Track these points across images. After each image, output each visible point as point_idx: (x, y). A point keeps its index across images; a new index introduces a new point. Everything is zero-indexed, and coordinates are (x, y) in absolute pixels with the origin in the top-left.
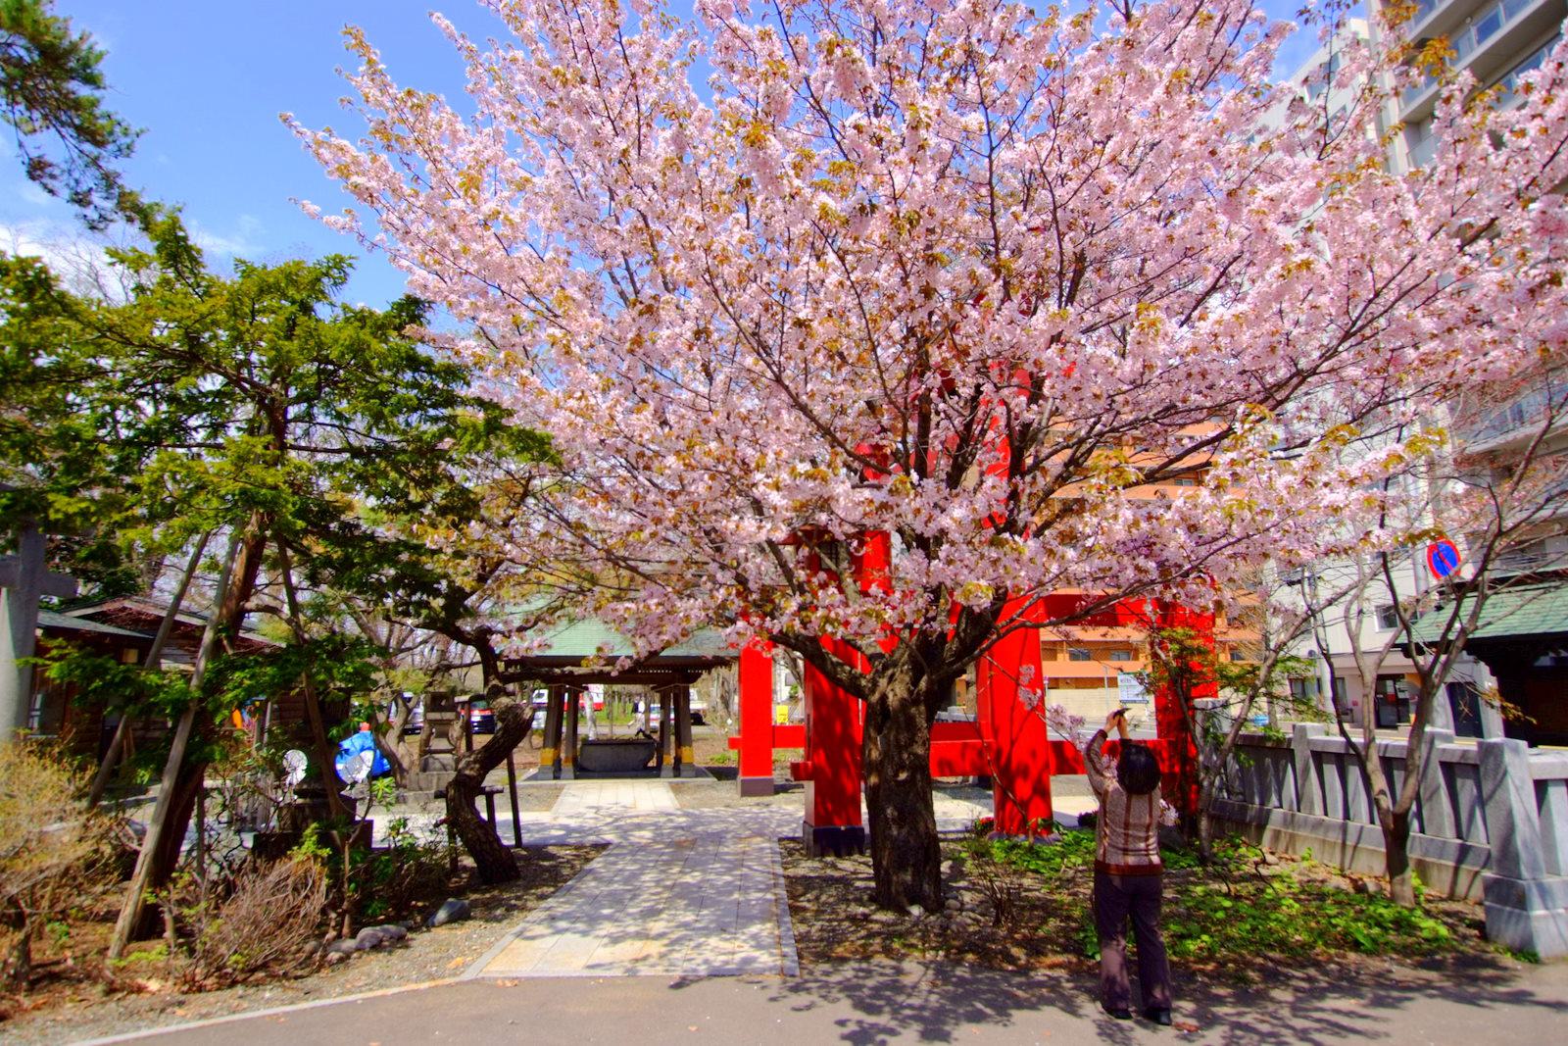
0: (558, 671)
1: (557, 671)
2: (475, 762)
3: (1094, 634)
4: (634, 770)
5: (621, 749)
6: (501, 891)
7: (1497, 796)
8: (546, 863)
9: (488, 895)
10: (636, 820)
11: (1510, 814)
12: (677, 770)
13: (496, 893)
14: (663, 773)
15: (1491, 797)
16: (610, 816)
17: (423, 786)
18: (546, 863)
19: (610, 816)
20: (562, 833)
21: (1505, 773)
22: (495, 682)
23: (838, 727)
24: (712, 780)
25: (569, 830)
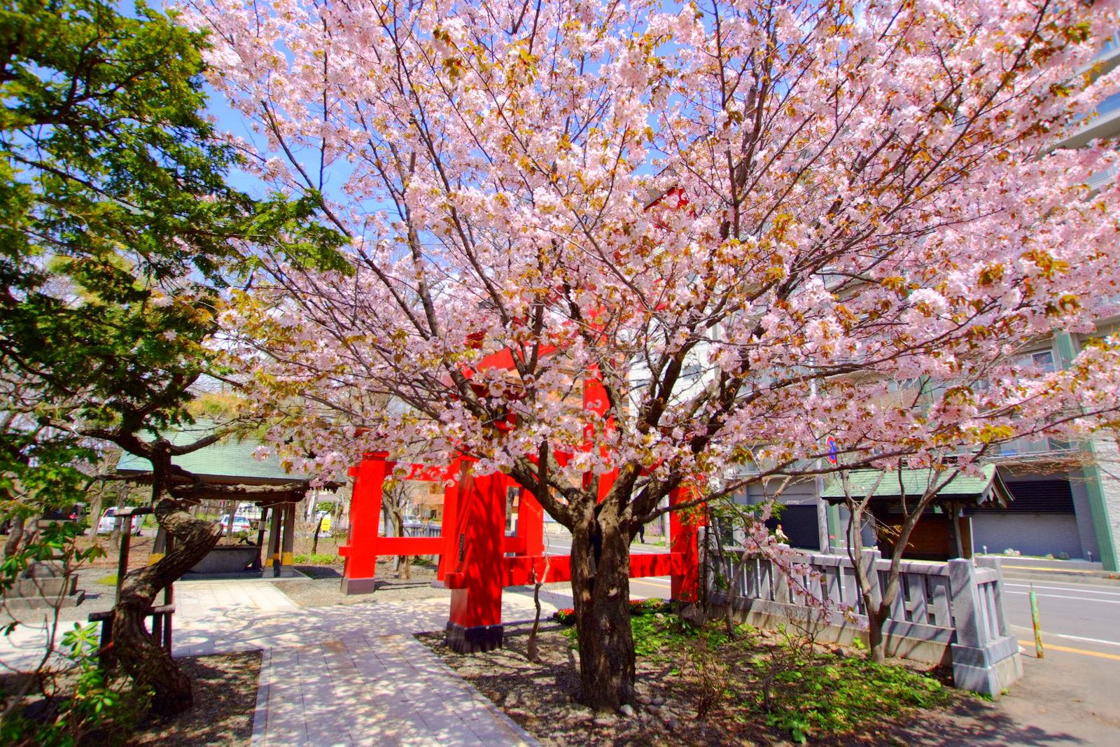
0: (231, 488)
1: (231, 488)
2: (146, 580)
3: (278, 488)
4: (237, 571)
5: (227, 554)
6: (182, 726)
7: (963, 593)
8: (212, 681)
9: (164, 734)
10: (273, 622)
11: (971, 605)
12: (278, 569)
13: (174, 729)
14: (265, 574)
15: (958, 592)
16: (243, 618)
17: (24, 592)
18: (212, 681)
19: (243, 618)
20: (204, 640)
21: (968, 580)
22: (168, 496)
23: (490, 545)
24: (307, 579)
25: (213, 637)
